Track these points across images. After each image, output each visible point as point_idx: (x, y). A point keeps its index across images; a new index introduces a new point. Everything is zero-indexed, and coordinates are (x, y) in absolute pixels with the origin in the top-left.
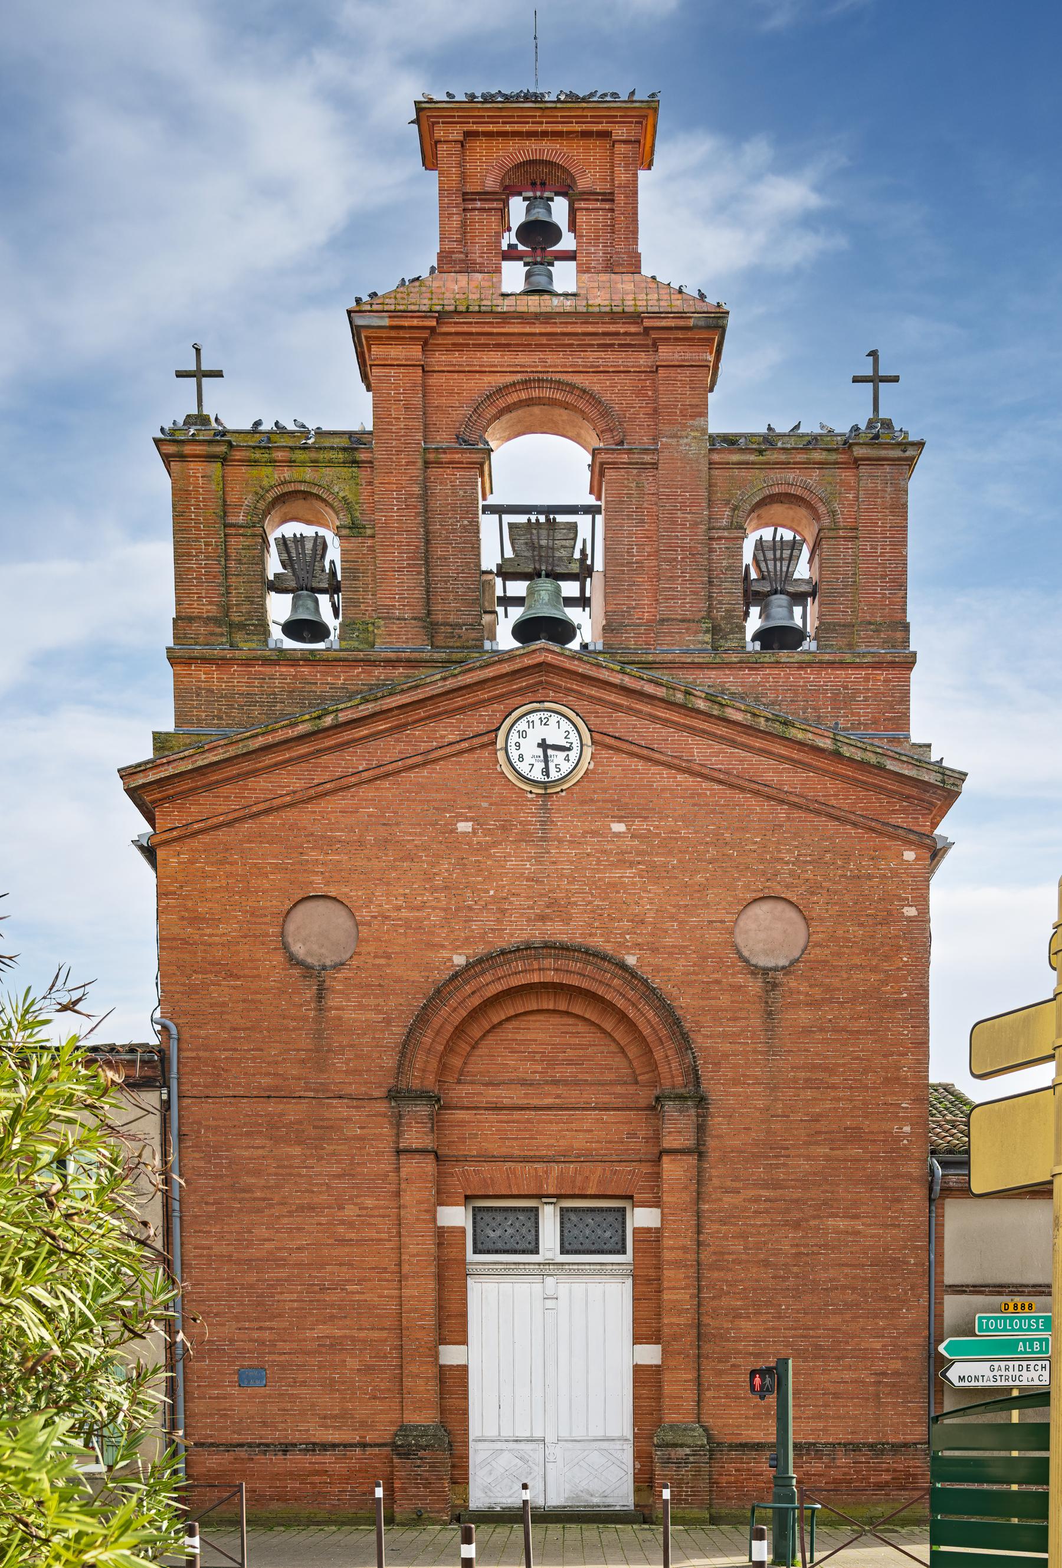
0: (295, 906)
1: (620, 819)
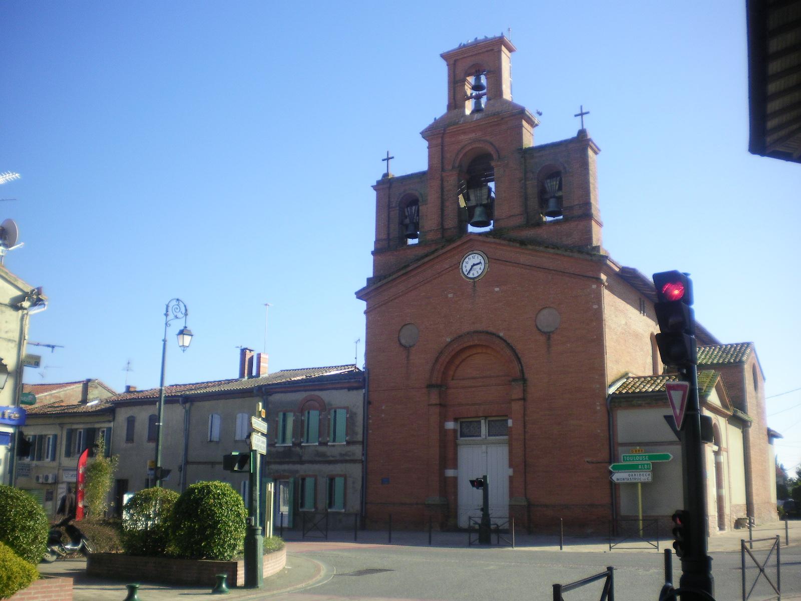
0: (402, 327)
1: (497, 286)
